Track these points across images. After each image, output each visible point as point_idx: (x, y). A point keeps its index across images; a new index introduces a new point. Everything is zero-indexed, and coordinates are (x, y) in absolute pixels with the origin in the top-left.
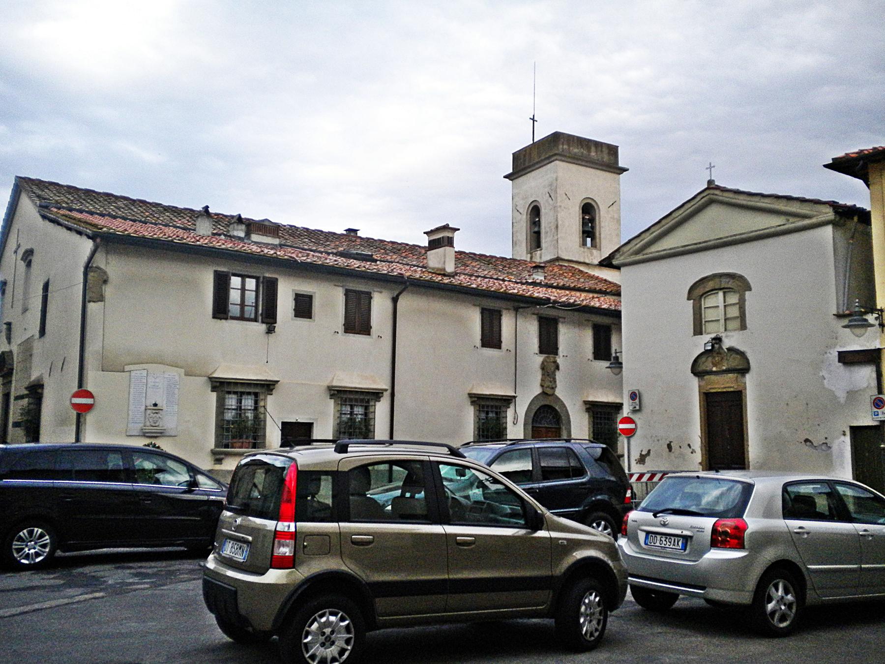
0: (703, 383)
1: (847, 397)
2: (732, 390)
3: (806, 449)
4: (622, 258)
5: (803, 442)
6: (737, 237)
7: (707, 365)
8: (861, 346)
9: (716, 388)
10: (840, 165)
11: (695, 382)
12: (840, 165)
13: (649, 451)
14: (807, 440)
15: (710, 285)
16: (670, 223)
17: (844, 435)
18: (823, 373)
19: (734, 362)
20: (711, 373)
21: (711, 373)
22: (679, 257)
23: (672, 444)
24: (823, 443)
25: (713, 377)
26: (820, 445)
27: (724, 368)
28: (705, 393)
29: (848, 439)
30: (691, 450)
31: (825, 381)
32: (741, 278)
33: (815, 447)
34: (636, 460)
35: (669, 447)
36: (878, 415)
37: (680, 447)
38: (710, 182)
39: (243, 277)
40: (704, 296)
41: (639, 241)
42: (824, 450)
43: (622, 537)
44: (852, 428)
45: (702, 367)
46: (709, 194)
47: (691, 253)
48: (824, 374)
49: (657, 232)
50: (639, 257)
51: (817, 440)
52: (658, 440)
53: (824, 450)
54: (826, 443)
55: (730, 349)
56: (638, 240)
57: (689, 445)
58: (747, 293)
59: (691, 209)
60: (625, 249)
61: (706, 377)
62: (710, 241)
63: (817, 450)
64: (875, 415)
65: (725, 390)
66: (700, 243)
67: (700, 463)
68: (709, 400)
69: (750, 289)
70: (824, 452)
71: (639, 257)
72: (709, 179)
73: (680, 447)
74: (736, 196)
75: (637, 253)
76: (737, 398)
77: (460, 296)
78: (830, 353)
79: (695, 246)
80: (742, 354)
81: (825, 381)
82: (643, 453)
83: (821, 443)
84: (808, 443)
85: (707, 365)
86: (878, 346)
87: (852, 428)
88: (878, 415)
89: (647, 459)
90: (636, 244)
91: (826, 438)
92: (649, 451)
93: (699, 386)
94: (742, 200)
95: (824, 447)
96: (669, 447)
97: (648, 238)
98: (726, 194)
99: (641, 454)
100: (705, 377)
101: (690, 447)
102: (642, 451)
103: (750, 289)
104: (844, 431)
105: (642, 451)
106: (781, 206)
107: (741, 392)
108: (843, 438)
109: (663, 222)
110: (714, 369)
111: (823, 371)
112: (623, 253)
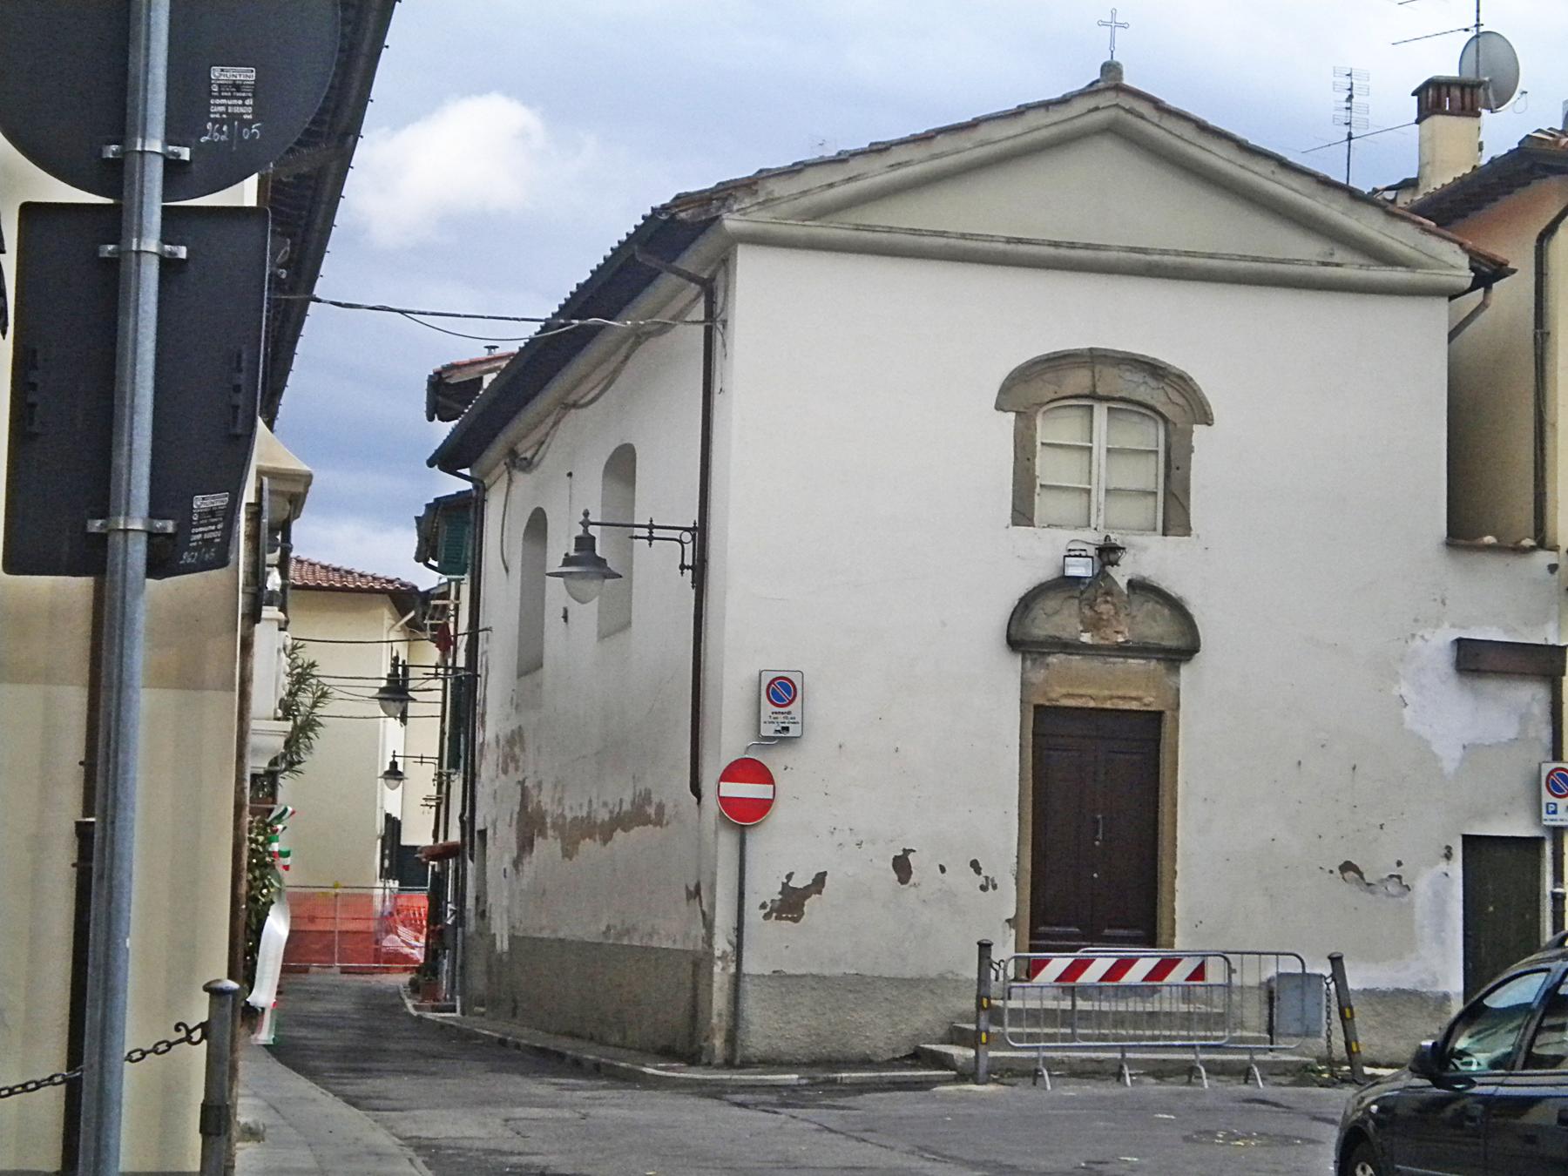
0: (1038, 676)
1: (1463, 760)
2: (1134, 706)
3: (1345, 890)
5: (1337, 871)
6: (144, 28)
8: (1506, 632)
9: (1081, 696)
11: (1010, 669)
13: (820, 880)
14: (1347, 867)
15: (1145, 390)
16: (969, 149)
17: (1448, 855)
18: (1404, 689)
19: (1157, 628)
20: (1070, 647)
21: (1070, 647)
22: (976, 265)
23: (911, 857)
24: (1391, 876)
26: (1382, 881)
27: (1121, 639)
29: (1456, 868)
30: (981, 880)
31: (1407, 712)
32: (1181, 383)
33: (1369, 884)
34: (763, 906)
35: (902, 867)
36: (1555, 812)
37: (943, 869)
38: (1111, 70)
39: (256, 90)
40: (1045, 408)
41: (841, 177)
42: (1393, 896)
43: (1530, 1004)
44: (1468, 840)
45: (1043, 625)
46: (1116, 105)
47: (1048, 268)
48: (1404, 691)
49: (920, 164)
51: (1376, 866)
52: (859, 845)
53: (1393, 896)
54: (1399, 877)
55: (1139, 587)
56: (837, 174)
59: (1290, 192)
60: (779, 188)
62: (1106, 248)
63: (1373, 893)
64: (1548, 813)
65: (1108, 705)
66: (1072, 246)
70: (1390, 900)
72: (1109, 59)
73: (943, 869)
74: (1203, 140)
75: (821, 213)
78: (1422, 637)
79: (1052, 251)
80: (1177, 607)
81: (1407, 712)
82: (798, 882)
83: (1385, 876)
84: (1351, 874)
86: (1553, 640)
87: (1468, 840)
88: (1555, 812)
90: (831, 185)
91: (1399, 864)
94: (1219, 158)
95: (1393, 888)
96: (902, 867)
97: (877, 174)
98: (1169, 123)
99: (785, 885)
100: (1052, 659)
101: (977, 869)
102: (789, 877)
103: (1207, 419)
104: (1449, 848)
105: (789, 877)
106: (1334, 210)
108: (1443, 866)
109: (942, 144)
110: (1086, 638)
111: (1403, 683)
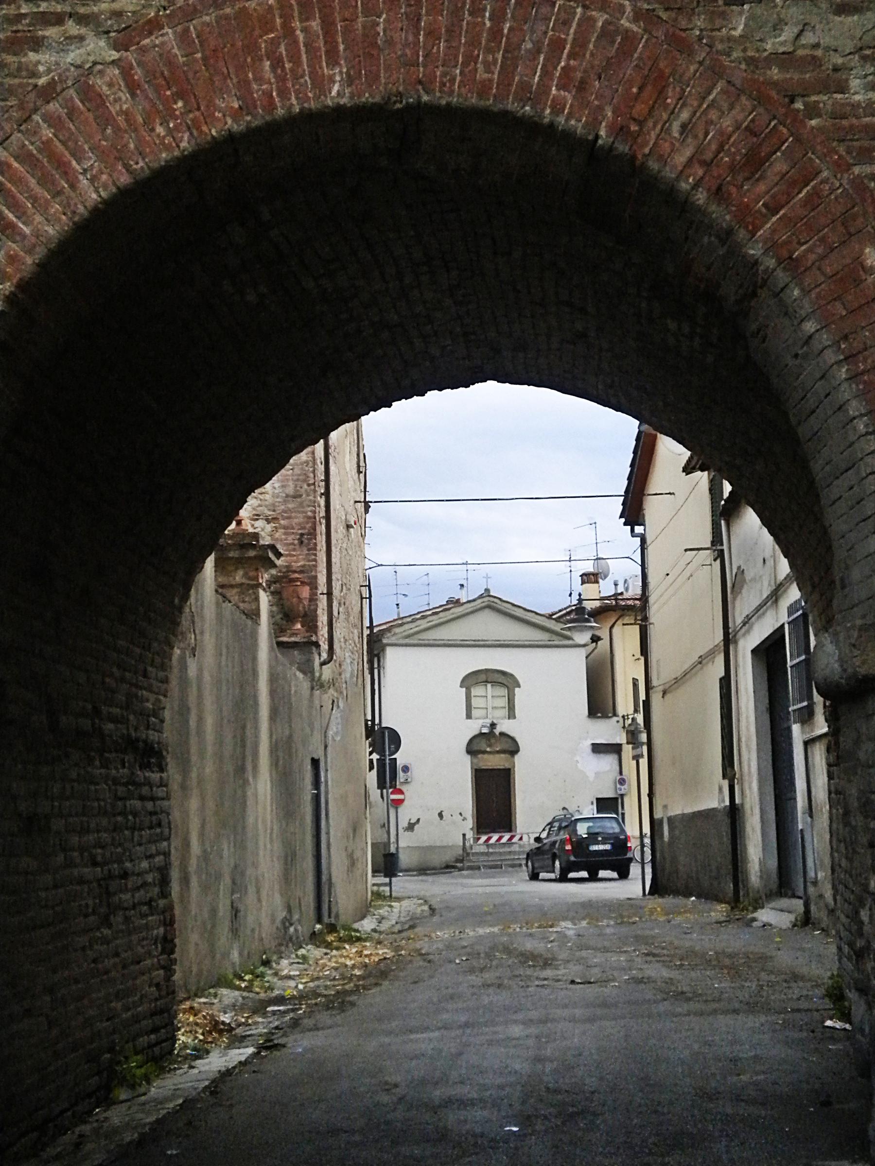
0: (475, 761)
4: (394, 638)
7: (483, 745)
10: (284, 1046)
11: (467, 759)
12: (284, 1046)
13: (418, 820)
18: (578, 758)
20: (485, 752)
25: (486, 756)
28: (476, 770)
35: (441, 815)
38: (487, 590)
44: (597, 799)
45: (475, 748)
50: (407, 641)
55: (502, 734)
57: (461, 814)
58: (517, 689)
61: (480, 756)
67: (472, 829)
68: (481, 777)
69: (519, 686)
71: (407, 641)
76: (505, 777)
77: (602, 616)
80: (513, 740)
82: (412, 821)
85: (483, 745)
87: (597, 799)
89: (416, 827)
92: (418, 820)
93: (472, 763)
94: (519, 613)
96: (441, 815)
103: (519, 686)
107: (509, 769)
110: (488, 749)
112: (395, 634)
